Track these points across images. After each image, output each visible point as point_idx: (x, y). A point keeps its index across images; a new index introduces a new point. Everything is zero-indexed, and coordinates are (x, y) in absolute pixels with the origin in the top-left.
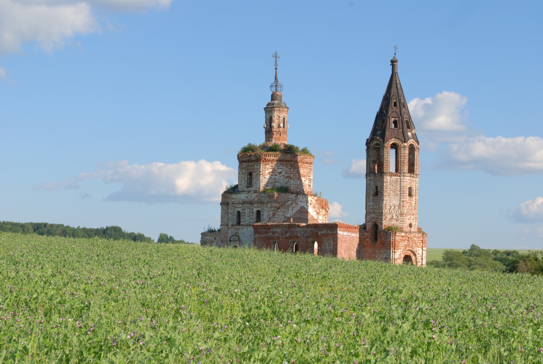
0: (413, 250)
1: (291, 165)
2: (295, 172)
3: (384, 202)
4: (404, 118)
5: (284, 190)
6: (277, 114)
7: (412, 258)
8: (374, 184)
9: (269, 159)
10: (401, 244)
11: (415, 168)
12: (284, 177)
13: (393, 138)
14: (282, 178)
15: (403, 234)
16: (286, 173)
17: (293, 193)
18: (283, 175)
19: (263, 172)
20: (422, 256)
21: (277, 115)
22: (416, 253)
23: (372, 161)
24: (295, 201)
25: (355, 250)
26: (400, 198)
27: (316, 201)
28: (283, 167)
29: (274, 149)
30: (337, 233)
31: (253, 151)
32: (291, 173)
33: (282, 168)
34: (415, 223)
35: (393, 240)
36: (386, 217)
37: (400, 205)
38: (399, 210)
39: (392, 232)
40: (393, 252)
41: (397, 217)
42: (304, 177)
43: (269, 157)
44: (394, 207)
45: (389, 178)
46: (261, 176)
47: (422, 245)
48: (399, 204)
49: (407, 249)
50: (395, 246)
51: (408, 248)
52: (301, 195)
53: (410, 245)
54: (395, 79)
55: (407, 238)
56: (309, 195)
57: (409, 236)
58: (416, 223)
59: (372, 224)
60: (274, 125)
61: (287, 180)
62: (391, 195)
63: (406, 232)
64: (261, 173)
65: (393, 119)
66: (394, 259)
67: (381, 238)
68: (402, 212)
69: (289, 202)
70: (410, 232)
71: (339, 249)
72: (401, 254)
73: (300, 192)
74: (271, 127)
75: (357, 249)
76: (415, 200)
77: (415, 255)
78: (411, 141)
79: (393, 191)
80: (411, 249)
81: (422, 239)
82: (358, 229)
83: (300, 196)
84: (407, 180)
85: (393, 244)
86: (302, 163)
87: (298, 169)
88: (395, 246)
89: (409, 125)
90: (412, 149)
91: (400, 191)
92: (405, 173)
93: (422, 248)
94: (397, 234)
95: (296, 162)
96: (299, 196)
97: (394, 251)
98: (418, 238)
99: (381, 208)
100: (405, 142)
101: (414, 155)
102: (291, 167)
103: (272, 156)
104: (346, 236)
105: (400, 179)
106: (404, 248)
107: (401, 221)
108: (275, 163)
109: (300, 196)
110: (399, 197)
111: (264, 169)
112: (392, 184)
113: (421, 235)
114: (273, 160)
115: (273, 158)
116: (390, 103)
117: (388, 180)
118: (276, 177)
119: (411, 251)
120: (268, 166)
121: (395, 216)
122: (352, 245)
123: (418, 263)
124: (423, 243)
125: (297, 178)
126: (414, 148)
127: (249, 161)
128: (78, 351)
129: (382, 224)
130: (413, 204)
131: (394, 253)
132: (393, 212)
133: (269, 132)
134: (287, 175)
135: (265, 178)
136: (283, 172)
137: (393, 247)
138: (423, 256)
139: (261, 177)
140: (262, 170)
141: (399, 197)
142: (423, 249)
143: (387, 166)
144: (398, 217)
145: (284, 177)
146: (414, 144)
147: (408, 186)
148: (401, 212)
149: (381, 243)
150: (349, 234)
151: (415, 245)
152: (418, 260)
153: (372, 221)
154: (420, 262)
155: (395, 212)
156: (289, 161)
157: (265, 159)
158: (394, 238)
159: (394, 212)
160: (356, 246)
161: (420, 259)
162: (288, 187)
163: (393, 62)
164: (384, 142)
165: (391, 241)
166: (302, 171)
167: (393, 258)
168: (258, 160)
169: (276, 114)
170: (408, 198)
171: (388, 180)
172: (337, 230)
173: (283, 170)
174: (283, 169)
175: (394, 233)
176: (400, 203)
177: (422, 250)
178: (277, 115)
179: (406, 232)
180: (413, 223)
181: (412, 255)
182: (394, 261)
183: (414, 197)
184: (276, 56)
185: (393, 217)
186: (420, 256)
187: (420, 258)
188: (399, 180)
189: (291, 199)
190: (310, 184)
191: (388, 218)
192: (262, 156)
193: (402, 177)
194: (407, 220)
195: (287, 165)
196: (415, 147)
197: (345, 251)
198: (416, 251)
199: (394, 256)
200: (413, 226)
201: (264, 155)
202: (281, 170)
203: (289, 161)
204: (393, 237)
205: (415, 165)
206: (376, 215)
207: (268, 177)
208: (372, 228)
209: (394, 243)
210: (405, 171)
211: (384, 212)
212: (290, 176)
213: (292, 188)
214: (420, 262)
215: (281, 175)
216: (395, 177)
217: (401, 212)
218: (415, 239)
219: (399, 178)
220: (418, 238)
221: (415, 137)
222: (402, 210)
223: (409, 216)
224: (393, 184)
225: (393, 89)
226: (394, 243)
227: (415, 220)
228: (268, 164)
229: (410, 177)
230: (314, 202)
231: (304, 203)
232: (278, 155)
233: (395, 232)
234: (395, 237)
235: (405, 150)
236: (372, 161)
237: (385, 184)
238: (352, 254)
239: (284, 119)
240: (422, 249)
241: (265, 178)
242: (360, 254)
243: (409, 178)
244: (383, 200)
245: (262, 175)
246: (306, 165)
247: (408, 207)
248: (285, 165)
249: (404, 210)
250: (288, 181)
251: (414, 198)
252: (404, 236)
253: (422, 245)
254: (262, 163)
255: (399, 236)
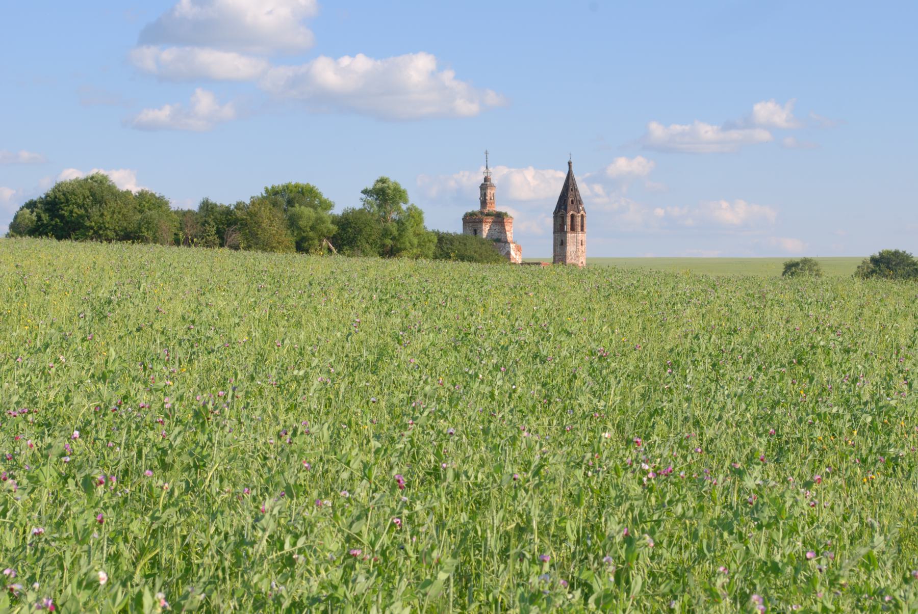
5: (498, 240)
24: (504, 247)
29: (488, 215)
31: (476, 215)
60: (488, 198)
65: (571, 213)
73: (506, 242)
74: (485, 199)
78: (582, 212)
84: (581, 236)
89: (580, 202)
90: (582, 216)
99: (565, 253)
127: (474, 222)
133: (484, 203)
163: (570, 163)
164: (566, 213)
166: (507, 228)
168: (481, 222)
169: (488, 191)
184: (486, 153)
221: (583, 209)
225: (570, 181)
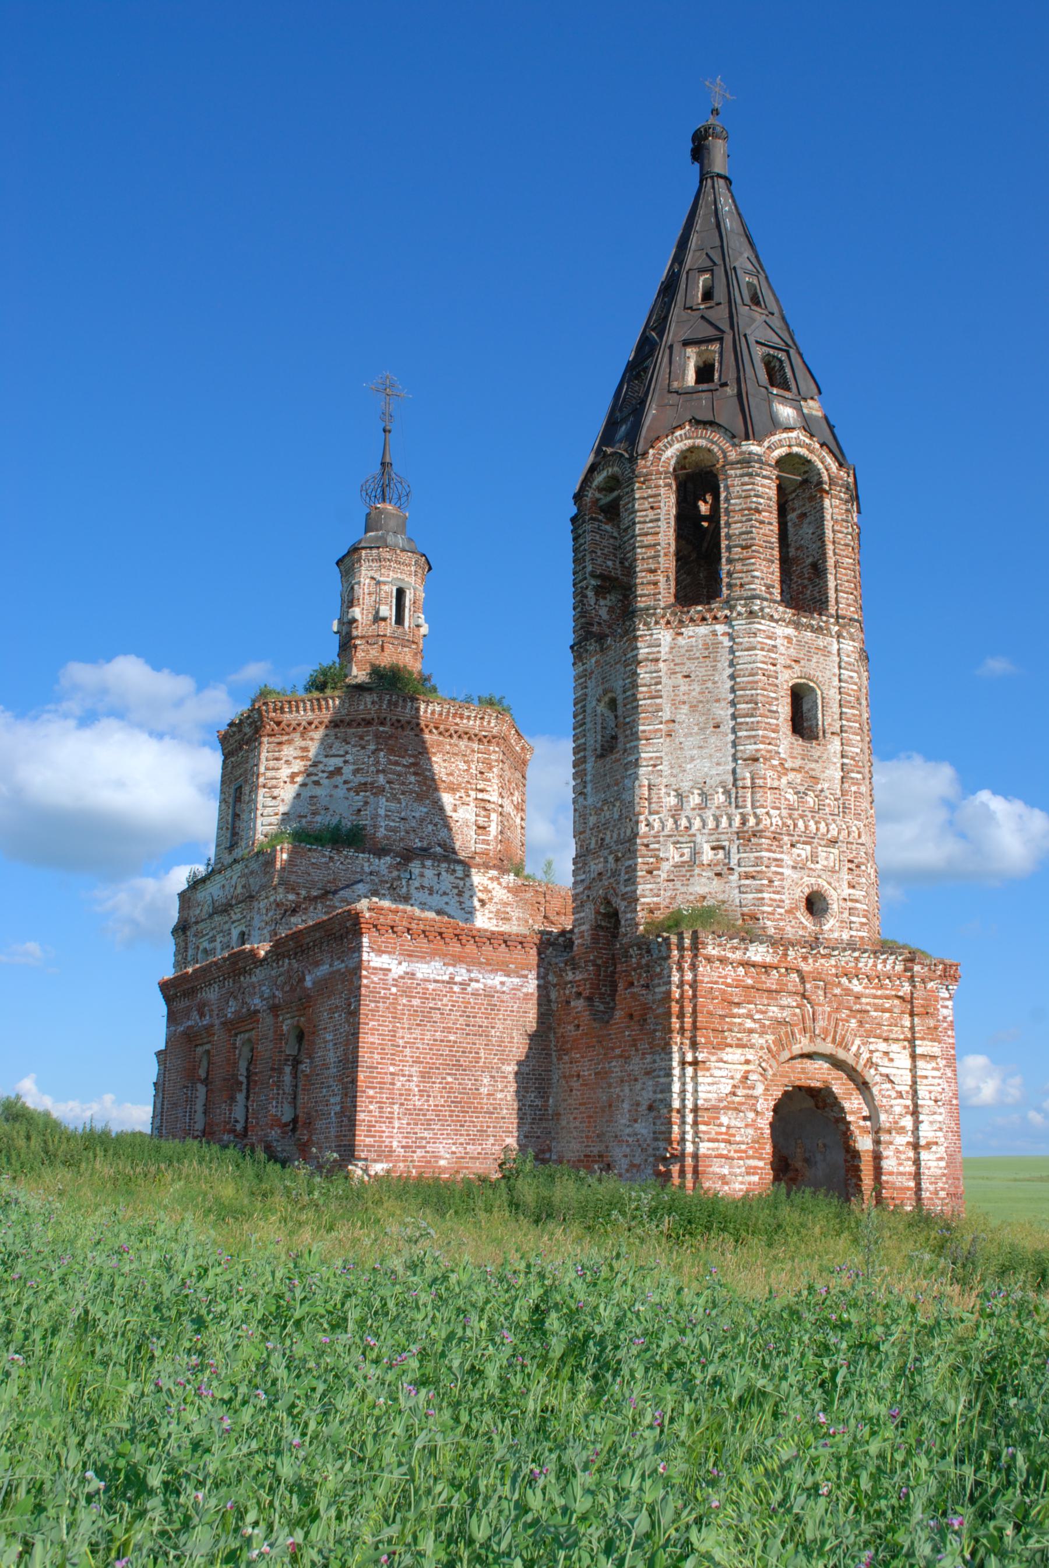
0: (841, 1054)
1: (377, 736)
2: (398, 768)
3: (642, 771)
4: (752, 340)
6: (371, 573)
7: (847, 1105)
8: (600, 691)
9: (294, 723)
10: (750, 1016)
11: (831, 584)
12: (349, 790)
13: (680, 427)
14: (341, 792)
15: (758, 953)
16: (356, 772)
17: (381, 852)
18: (345, 782)
19: (269, 774)
20: (915, 1092)
21: (373, 578)
22: (870, 1075)
23: (593, 575)
25: (511, 1068)
26: (734, 744)
27: (514, 891)
28: (348, 747)
30: (359, 966)
32: (378, 771)
33: (342, 753)
34: (847, 892)
35: (681, 985)
36: (659, 859)
37: (735, 780)
38: (732, 810)
39: (674, 939)
40: (683, 1063)
41: (721, 854)
42: (452, 789)
43: (295, 714)
44: (703, 794)
45: (665, 636)
46: (262, 791)
47: (912, 1028)
48: (730, 779)
49: (796, 1049)
50: (695, 1027)
51: (804, 1044)
52: (428, 863)
53: (821, 1024)
54: (711, 198)
55: (794, 976)
56: (478, 866)
57: (805, 968)
58: (858, 894)
59: (598, 912)
61: (358, 800)
62: (680, 731)
63: (778, 943)
64: (261, 780)
66: (695, 1110)
67: (632, 984)
68: (752, 821)
69: (360, 886)
70: (814, 943)
71: (367, 1056)
72: (753, 1077)
75: (519, 1063)
76: (838, 760)
77: (863, 1086)
79: (693, 708)
80: (828, 1048)
81: (907, 988)
82: (534, 952)
83: (423, 866)
85: (681, 1016)
86: (440, 733)
87: (422, 752)
88: (695, 1027)
91: (733, 703)
92: (755, 597)
93: (912, 1041)
94: (711, 950)
95: (415, 727)
96: (415, 867)
97: (689, 1058)
98: (876, 979)
100: (747, 438)
101: (822, 518)
102: (378, 744)
103: (305, 710)
104: (431, 986)
105: (732, 638)
106: (770, 1038)
107: (748, 876)
108: (318, 735)
109: (423, 866)
110: (732, 737)
111: (272, 763)
112: (685, 670)
113: (899, 968)
114: (310, 723)
115: (310, 716)
116: (683, 286)
117: (664, 650)
118: (318, 791)
119: (837, 1064)
120: (288, 751)
121: (706, 847)
122: (480, 1042)
123: (884, 1137)
124: (912, 1014)
125: (411, 792)
126: (820, 483)
128: (231, 1411)
129: (632, 899)
130: (831, 780)
131: (690, 1070)
132: (697, 823)
134: (360, 779)
135: (274, 798)
136: (348, 770)
137: (682, 1030)
138: (921, 1094)
139: (260, 798)
140: (267, 769)
141: (732, 737)
142: (919, 1051)
143: (651, 577)
144: (728, 855)
145: (349, 790)
146: (814, 458)
147: (787, 679)
148: (744, 822)
149: (631, 1016)
150: (461, 973)
151: (853, 1023)
152: (883, 1117)
153: (593, 894)
154: (902, 1130)
155: (711, 824)
156: (369, 723)
157: (278, 724)
158: (689, 976)
159: (704, 824)
160: (518, 1047)
161: (898, 1110)
162: (365, 826)
165: (668, 993)
166: (440, 766)
167: (689, 1104)
170: (786, 742)
171: (664, 650)
172: (359, 948)
173: (346, 762)
174: (349, 757)
175: (687, 942)
176: (734, 772)
177: (914, 1057)
178: (373, 578)
179: (778, 943)
180: (836, 894)
181: (840, 1086)
182: (696, 1123)
183: (837, 741)
185: (695, 853)
186: (900, 1095)
187: (899, 1106)
188: (727, 643)
189: (371, 873)
190: (481, 823)
191: (666, 866)
192: (267, 711)
193: (740, 624)
194: (787, 872)
195: (361, 738)
196: (826, 478)
197: (423, 1075)
198: (870, 1063)
199: (689, 1087)
200: (835, 906)
201: (271, 706)
202: (338, 762)
203: (369, 723)
204: (680, 969)
205: (831, 570)
206: (611, 858)
207: (288, 793)
208: (595, 939)
209: (689, 1009)
210: (759, 588)
211: (643, 828)
212: (372, 783)
213: (382, 832)
214: (902, 1130)
215: (339, 780)
216: (703, 630)
217: (744, 822)
218: (856, 987)
219: (720, 628)
220: (876, 979)
222: (749, 809)
223: (803, 851)
224: (690, 666)
226: (689, 1009)
227: (845, 876)
228: (290, 742)
229: (797, 626)
230: (500, 893)
231: (445, 899)
232: (327, 702)
233: (695, 936)
234: (694, 967)
235: (750, 475)
236: (593, 575)
237: (644, 674)
238: (484, 1090)
239: (400, 593)
240: (913, 1047)
241: (274, 798)
242: (543, 1092)
243: (790, 631)
244: (636, 764)
245: (264, 786)
246: (463, 744)
247: (792, 797)
248: (353, 741)
249: (759, 811)
250: (366, 803)
251: (835, 745)
252: (767, 968)
253: (907, 1023)
254: (265, 739)
255: (723, 960)
